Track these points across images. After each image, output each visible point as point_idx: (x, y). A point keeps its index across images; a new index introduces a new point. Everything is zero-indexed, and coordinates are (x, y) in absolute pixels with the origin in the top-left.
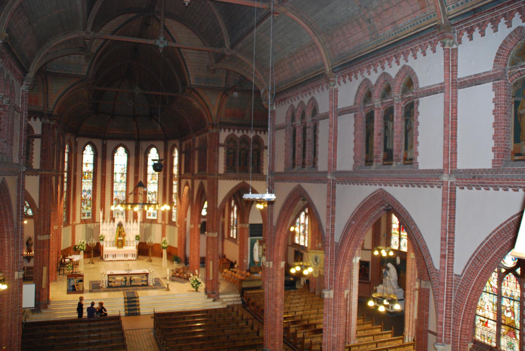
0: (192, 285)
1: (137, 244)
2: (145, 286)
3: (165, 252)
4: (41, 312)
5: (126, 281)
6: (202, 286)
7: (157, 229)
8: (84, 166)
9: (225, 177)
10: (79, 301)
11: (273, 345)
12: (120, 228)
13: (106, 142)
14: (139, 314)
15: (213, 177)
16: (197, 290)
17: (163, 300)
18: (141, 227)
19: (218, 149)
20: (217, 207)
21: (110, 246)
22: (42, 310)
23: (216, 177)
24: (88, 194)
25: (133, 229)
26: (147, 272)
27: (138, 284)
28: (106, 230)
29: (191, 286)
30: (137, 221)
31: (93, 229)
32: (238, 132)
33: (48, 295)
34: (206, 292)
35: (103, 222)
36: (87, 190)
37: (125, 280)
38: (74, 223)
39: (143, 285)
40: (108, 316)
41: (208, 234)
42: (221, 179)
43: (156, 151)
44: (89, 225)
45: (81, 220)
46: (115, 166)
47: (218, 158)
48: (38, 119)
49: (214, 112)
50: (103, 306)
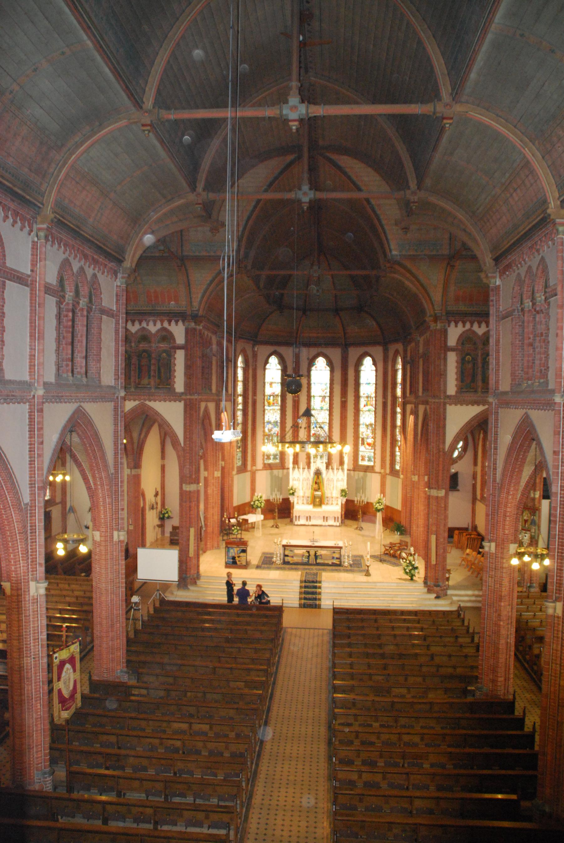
0: (405, 570)
1: (344, 503)
2: (337, 565)
3: (379, 516)
4: (188, 589)
5: (309, 556)
6: (420, 574)
7: (374, 481)
8: (267, 386)
9: (457, 400)
10: (227, 579)
12: (318, 478)
14: (318, 607)
15: (437, 401)
17: (356, 589)
18: (349, 476)
19: (445, 355)
20: (444, 449)
21: (303, 503)
22: (189, 587)
24: (275, 427)
26: (341, 544)
27: (326, 562)
28: (298, 480)
29: (403, 571)
30: (343, 469)
31: (282, 478)
32: (480, 327)
33: (198, 566)
34: (425, 583)
35: (294, 468)
36: (272, 421)
37: (308, 555)
38: (254, 468)
40: (272, 604)
41: (430, 492)
42: (450, 405)
44: (275, 472)
45: (265, 464)
47: (445, 370)
48: (180, 323)
49: (437, 296)
50: (262, 589)
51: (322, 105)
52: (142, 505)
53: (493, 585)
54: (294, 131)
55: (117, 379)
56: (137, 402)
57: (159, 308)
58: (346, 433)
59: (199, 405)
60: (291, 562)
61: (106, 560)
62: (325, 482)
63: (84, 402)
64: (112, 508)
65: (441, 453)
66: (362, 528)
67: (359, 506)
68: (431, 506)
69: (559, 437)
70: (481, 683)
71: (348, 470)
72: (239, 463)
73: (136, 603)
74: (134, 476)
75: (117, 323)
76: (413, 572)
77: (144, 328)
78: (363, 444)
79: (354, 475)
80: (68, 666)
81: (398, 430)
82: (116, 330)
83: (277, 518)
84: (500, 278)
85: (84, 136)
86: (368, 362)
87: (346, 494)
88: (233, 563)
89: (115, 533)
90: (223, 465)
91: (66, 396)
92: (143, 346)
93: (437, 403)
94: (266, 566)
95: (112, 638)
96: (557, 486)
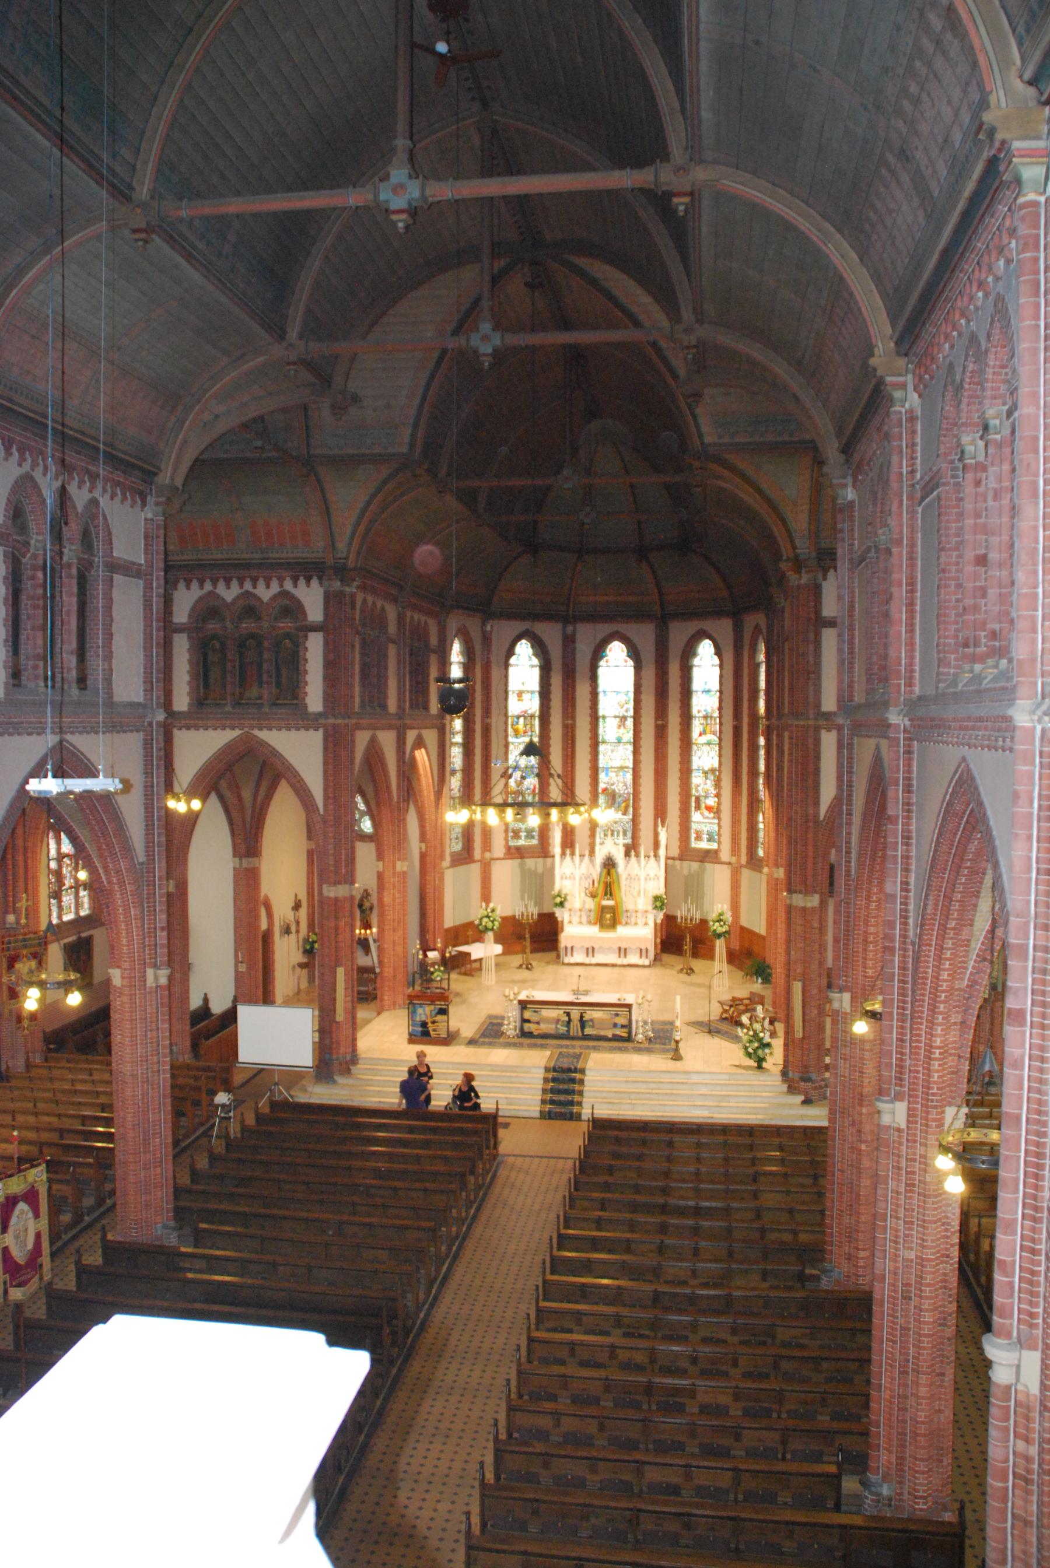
0: (746, 1048)
1: (659, 921)
4: (334, 1082)
6: (775, 1058)
7: (718, 878)
8: (512, 700)
11: (849, 1258)
12: (609, 873)
13: (575, 629)
15: (801, 723)
16: (760, 1067)
20: (816, 815)
21: (580, 923)
22: (336, 1078)
23: (811, 722)
25: (647, 878)
26: (629, 999)
27: (602, 1033)
28: (572, 877)
30: (656, 856)
31: (543, 873)
32: (228, 587)
34: (784, 1073)
35: (563, 854)
38: (487, 855)
39: (616, 1038)
41: (791, 898)
43: (712, 650)
44: (530, 863)
45: (508, 848)
46: (601, 697)
47: (818, 664)
48: (315, 582)
50: (474, 1083)
51: (451, 179)
52: (264, 926)
53: (847, 1075)
54: (402, 231)
55: (148, 691)
56: (237, 733)
57: (275, 555)
58: (666, 786)
59: (352, 735)
60: (535, 1033)
61: (132, 1020)
62: (623, 882)
63: (72, 733)
64: (143, 926)
65: (811, 824)
66: (691, 969)
67: (686, 927)
68: (793, 926)
69: (898, 790)
70: (831, 1262)
71: (667, 858)
72: (458, 847)
73: (223, 1106)
74: (247, 870)
75: (148, 587)
76: (760, 1052)
77: (247, 592)
78: (698, 807)
79: (682, 867)
80: (22, 1206)
81: (761, 781)
82: (145, 601)
83: (528, 950)
84: (854, 487)
85: (32, 253)
86: (706, 649)
87: (663, 904)
88: (422, 1034)
89: (150, 972)
90: (423, 850)
91: (30, 723)
92: (248, 626)
93: (803, 726)
94: (487, 1040)
95: (145, 1165)
96: (896, 882)
